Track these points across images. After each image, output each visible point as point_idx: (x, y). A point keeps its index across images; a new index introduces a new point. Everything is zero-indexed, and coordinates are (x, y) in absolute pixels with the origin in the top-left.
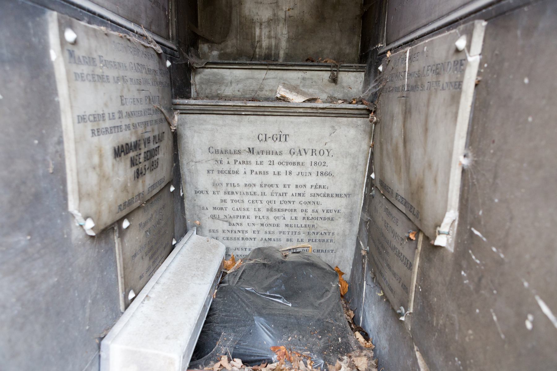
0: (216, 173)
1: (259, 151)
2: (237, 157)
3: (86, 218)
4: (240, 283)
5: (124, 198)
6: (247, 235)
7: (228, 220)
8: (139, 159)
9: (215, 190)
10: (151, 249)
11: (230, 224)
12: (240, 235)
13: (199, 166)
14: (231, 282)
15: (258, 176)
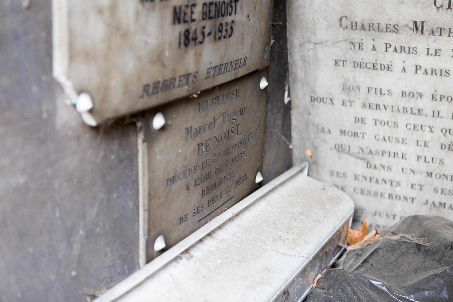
0: (349, 66)
1: (435, 28)
2: (390, 38)
3: (80, 92)
4: (362, 270)
5: (153, 74)
6: (398, 190)
7: (365, 157)
8: (192, 13)
9: (346, 98)
10: (208, 176)
11: (369, 165)
12: (387, 189)
13: (321, 52)
14: (347, 264)
15: (429, 77)
